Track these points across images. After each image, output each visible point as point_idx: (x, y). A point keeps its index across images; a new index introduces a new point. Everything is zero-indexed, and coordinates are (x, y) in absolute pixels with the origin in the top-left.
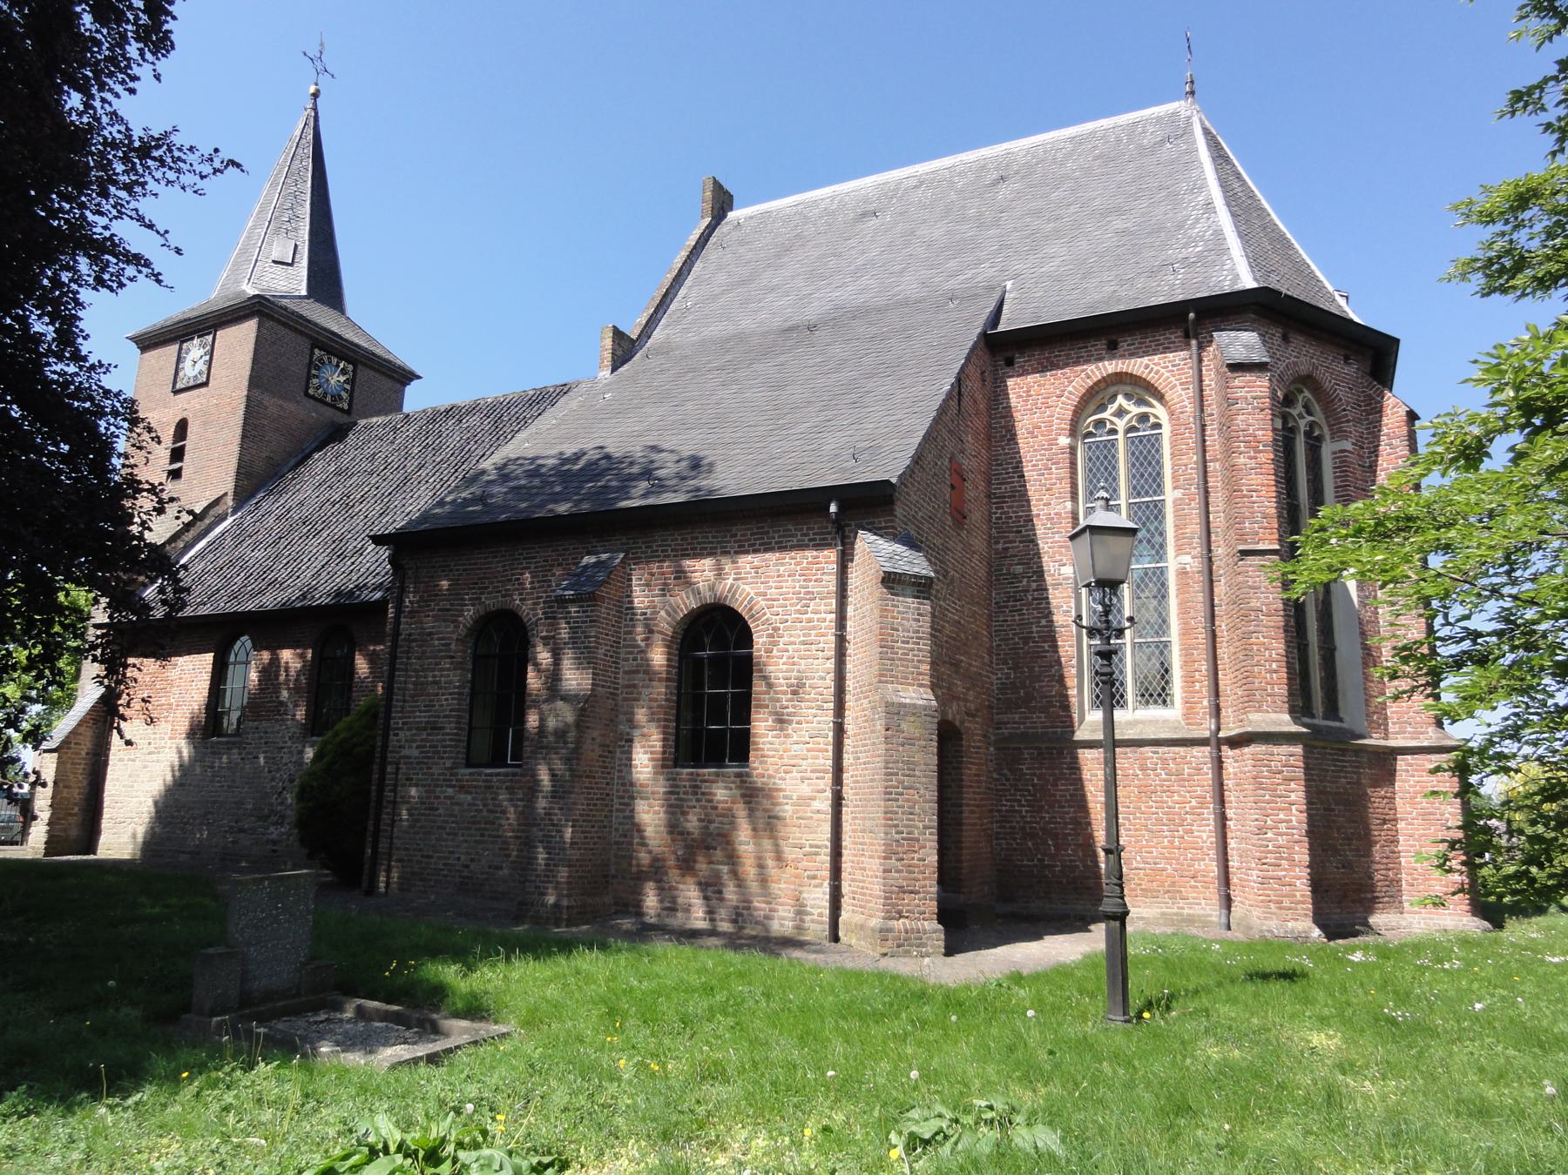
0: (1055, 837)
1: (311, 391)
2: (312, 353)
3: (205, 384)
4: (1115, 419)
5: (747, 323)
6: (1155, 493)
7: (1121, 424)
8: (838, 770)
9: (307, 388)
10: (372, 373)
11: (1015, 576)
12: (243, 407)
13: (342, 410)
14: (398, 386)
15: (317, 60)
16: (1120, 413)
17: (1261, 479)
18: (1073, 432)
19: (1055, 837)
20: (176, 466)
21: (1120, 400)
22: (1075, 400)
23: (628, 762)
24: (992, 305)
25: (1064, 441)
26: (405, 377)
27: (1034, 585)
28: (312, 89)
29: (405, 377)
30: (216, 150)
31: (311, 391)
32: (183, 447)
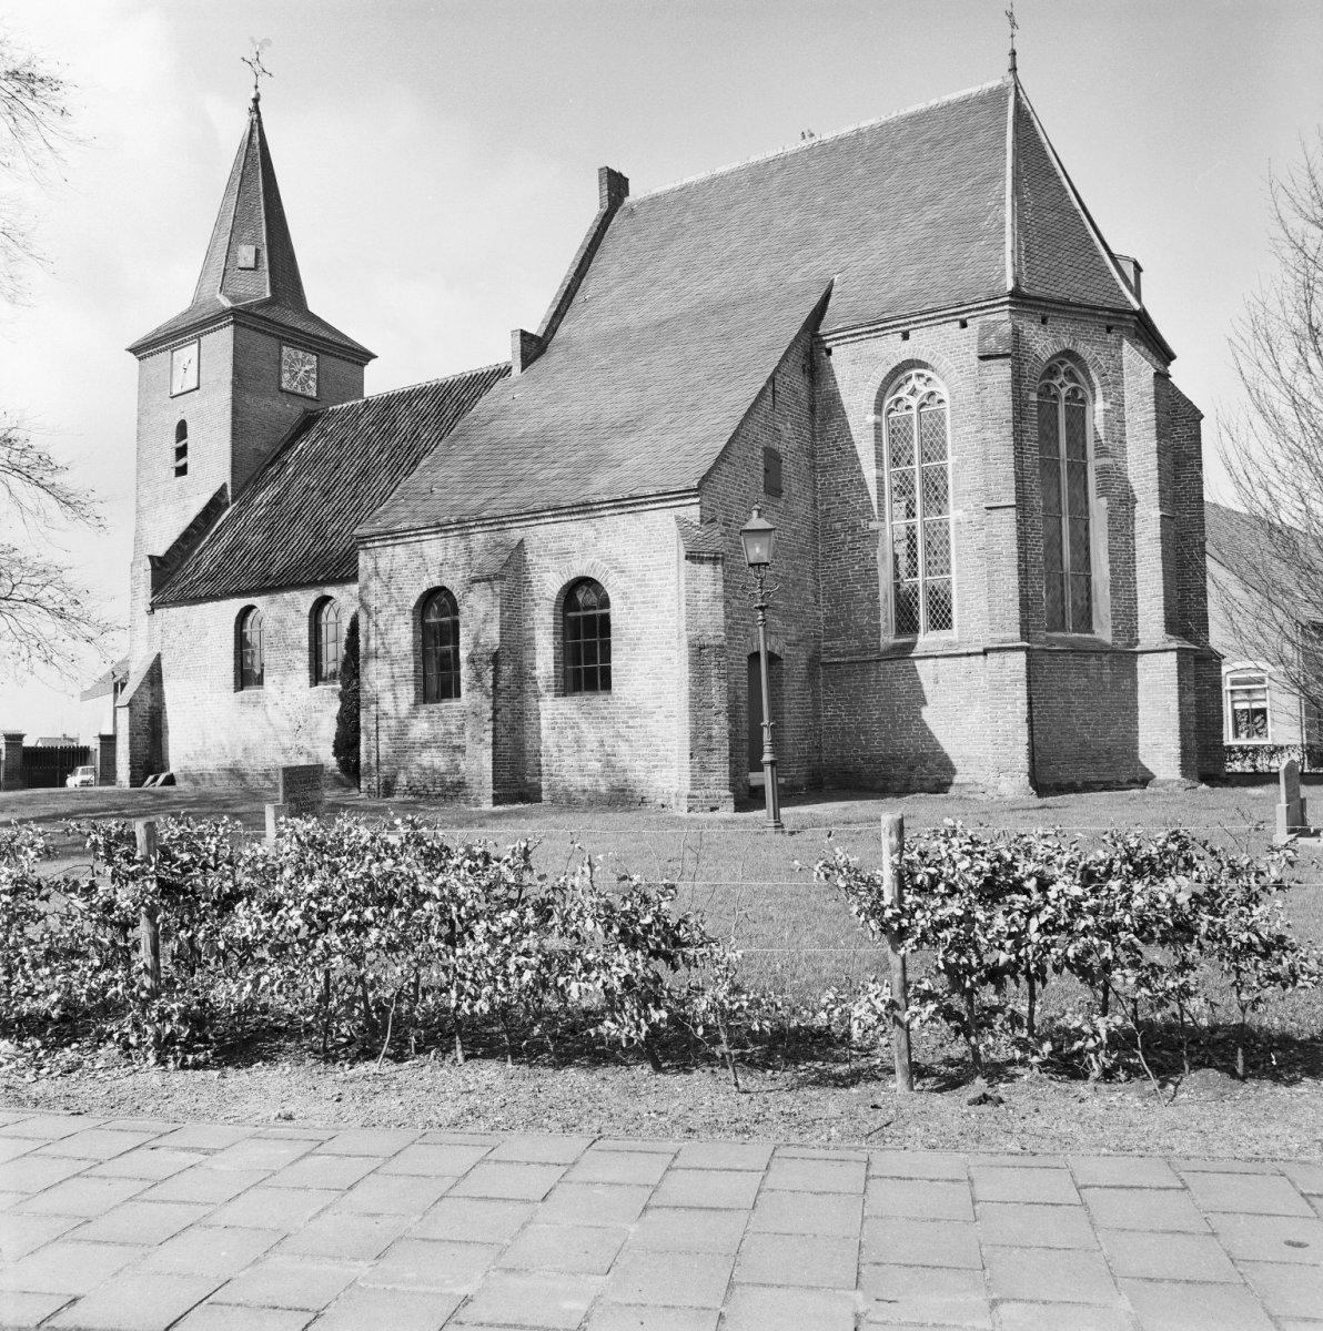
0: (865, 733)
1: (284, 385)
2: (280, 352)
3: (197, 388)
4: (910, 397)
5: (632, 318)
6: (941, 458)
7: (914, 402)
8: (969, 655)
9: (280, 382)
10: (333, 359)
11: (836, 531)
12: (230, 408)
13: (311, 399)
14: (357, 367)
15: (254, 63)
16: (913, 392)
17: (1002, 449)
18: (878, 410)
19: (865, 733)
20: (181, 462)
21: (914, 381)
22: (878, 383)
23: (71, 771)
24: (815, 299)
25: (871, 418)
26: (365, 357)
27: (849, 538)
28: (253, 95)
29: (365, 357)
30: (181, 471)
31: (284, 385)
32: (185, 446)
